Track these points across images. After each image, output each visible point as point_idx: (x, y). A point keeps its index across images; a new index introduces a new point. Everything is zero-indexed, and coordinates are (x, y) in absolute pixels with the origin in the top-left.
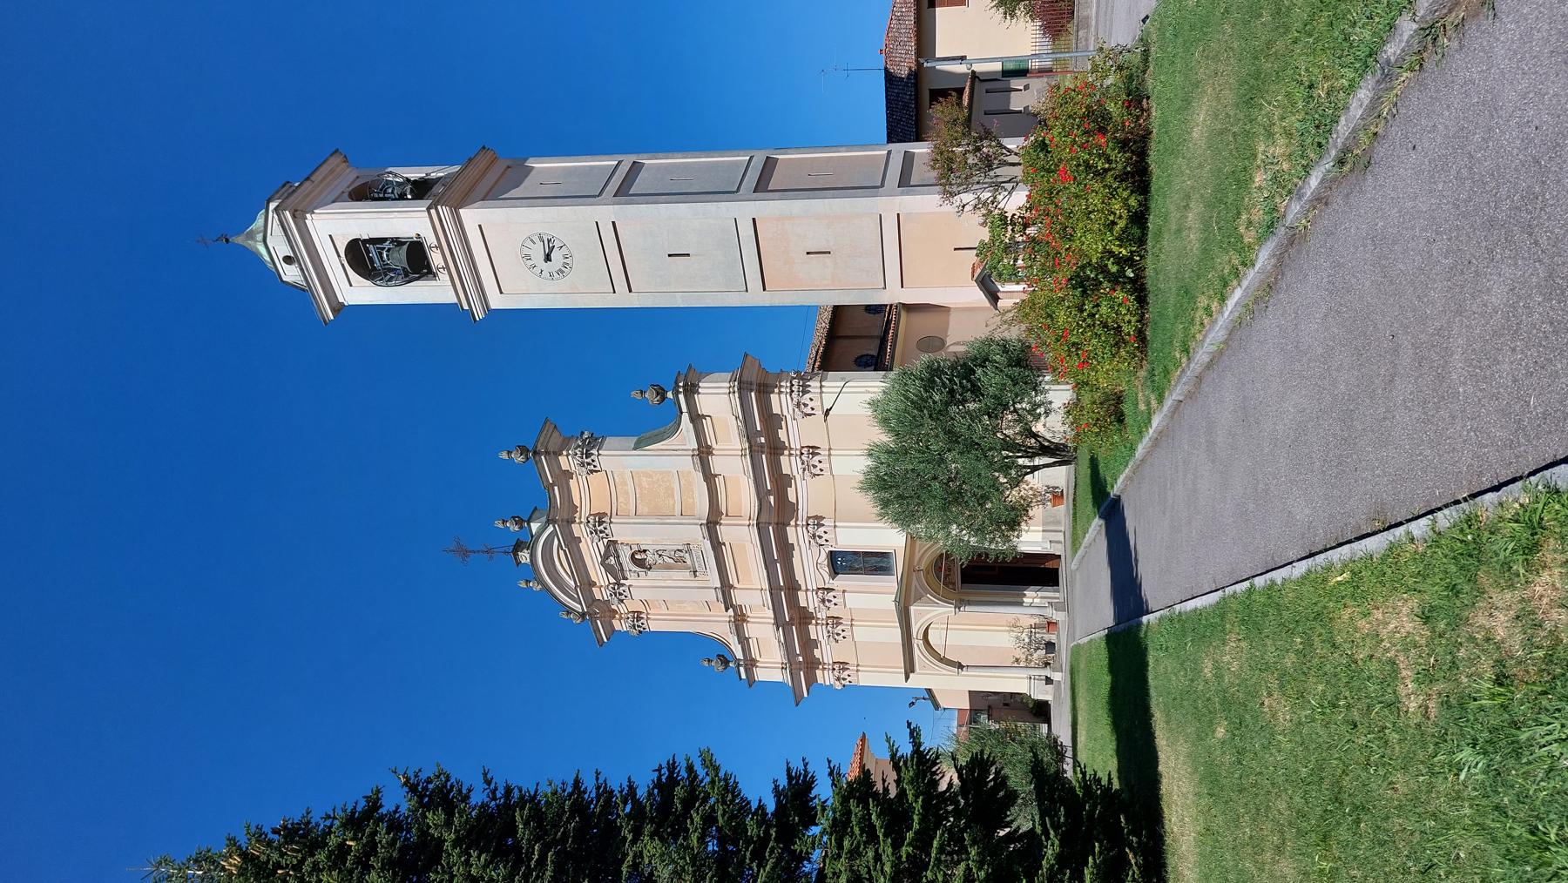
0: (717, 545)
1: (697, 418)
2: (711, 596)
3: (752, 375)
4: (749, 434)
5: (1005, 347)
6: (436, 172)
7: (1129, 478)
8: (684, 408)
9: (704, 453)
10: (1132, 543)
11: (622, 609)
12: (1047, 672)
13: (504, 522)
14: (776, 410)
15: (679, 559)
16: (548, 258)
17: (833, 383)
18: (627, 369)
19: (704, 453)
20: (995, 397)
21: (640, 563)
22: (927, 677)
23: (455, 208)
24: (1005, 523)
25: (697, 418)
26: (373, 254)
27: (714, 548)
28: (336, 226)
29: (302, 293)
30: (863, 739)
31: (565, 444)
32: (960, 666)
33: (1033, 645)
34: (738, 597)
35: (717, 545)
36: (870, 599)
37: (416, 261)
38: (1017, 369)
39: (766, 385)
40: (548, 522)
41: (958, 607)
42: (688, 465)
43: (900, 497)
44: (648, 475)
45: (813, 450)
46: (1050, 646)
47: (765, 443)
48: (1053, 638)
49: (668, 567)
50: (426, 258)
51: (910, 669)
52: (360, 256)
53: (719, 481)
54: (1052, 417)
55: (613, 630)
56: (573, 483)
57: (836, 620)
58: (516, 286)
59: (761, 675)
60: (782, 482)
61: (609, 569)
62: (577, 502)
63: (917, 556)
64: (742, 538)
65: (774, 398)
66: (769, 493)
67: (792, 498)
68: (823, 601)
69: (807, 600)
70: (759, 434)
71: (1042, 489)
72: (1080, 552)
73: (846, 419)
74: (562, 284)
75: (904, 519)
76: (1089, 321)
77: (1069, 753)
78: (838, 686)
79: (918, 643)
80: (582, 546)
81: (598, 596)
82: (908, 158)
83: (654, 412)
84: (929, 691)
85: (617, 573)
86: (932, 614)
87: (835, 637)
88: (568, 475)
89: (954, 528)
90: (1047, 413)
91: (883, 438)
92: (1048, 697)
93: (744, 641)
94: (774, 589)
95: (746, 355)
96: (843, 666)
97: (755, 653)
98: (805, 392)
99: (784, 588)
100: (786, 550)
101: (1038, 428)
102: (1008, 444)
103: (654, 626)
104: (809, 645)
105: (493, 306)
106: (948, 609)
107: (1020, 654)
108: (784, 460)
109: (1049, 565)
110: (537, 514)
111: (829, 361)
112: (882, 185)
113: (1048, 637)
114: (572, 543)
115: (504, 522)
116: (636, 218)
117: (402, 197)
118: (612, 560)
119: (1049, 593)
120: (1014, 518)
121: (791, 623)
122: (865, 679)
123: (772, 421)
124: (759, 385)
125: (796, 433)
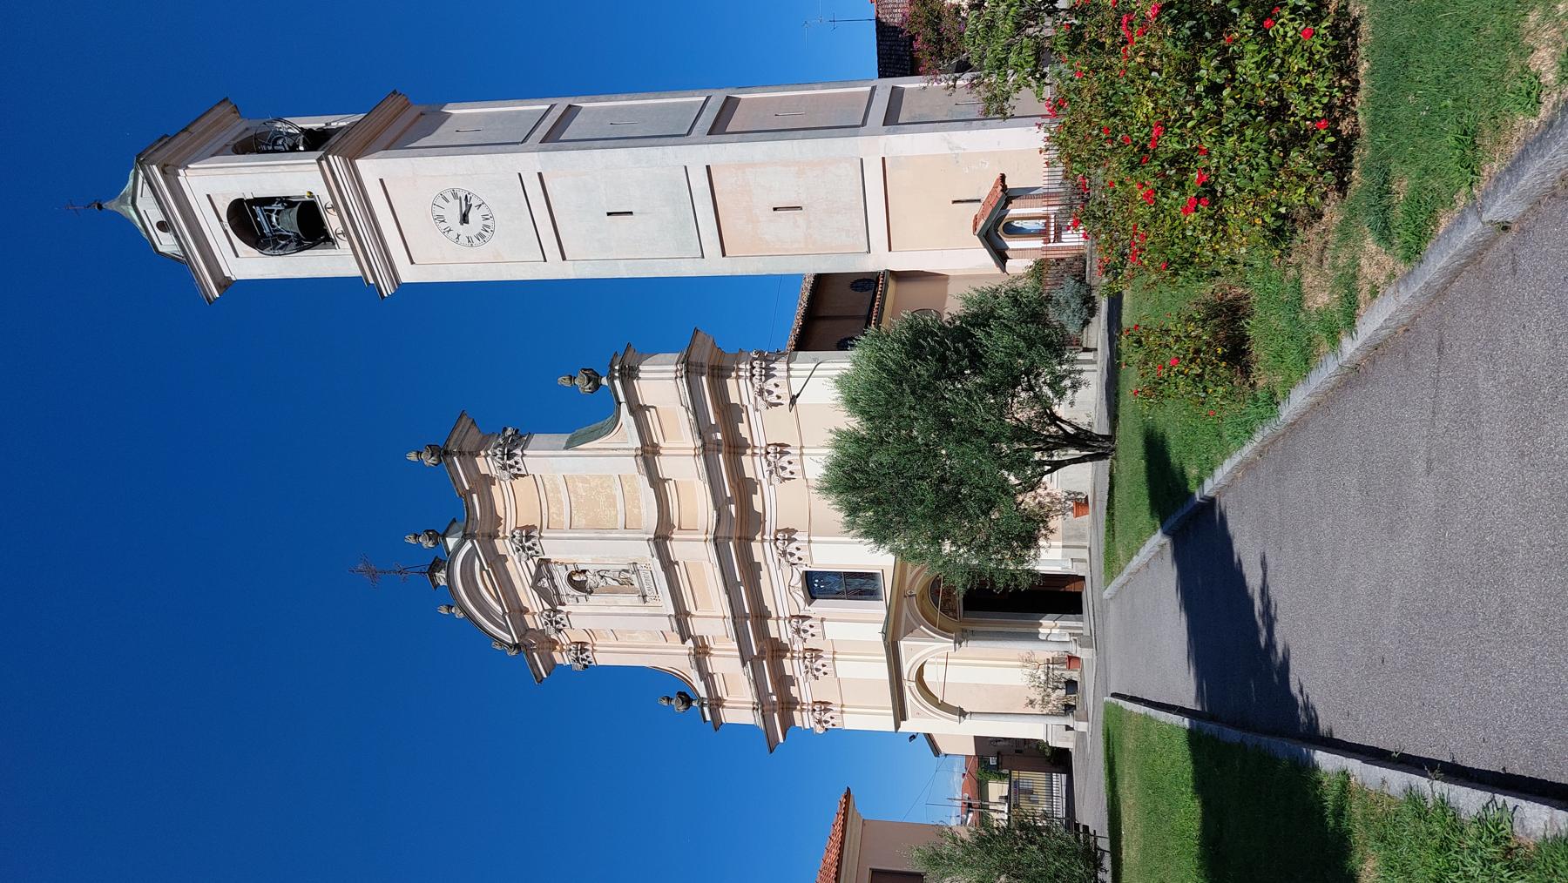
0: (668, 565)
1: (638, 410)
2: (666, 625)
3: (702, 355)
4: (702, 429)
5: (1015, 299)
6: (338, 121)
7: (1248, 466)
8: (622, 399)
9: (649, 453)
10: (1253, 581)
11: (563, 638)
12: (1070, 721)
13: (416, 536)
14: (734, 399)
15: (625, 581)
16: (464, 219)
17: (804, 363)
18: (555, 353)
19: (649, 453)
20: (1001, 366)
21: (580, 587)
22: (921, 720)
23: (351, 158)
24: (1018, 538)
25: (638, 410)
26: (261, 218)
27: (664, 568)
28: (214, 183)
29: (179, 266)
30: (848, 795)
31: (483, 444)
32: (962, 713)
33: (1050, 683)
34: (697, 627)
35: (668, 565)
36: (854, 629)
37: (309, 227)
38: (1033, 327)
39: (721, 368)
40: (465, 537)
41: (958, 641)
42: (631, 467)
43: (876, 502)
44: (584, 480)
45: (782, 449)
46: (1071, 685)
47: (723, 440)
48: (1075, 675)
49: (614, 591)
50: (323, 223)
51: (900, 714)
52: (246, 219)
53: (670, 487)
54: (1082, 391)
55: (554, 664)
56: (495, 489)
57: (816, 653)
58: (431, 256)
59: (729, 716)
60: (745, 488)
61: (543, 594)
62: (500, 513)
63: (909, 578)
64: (697, 556)
65: (731, 383)
66: (730, 501)
67: (758, 507)
68: (798, 631)
69: (779, 630)
70: (715, 428)
71: (1061, 495)
72: (1120, 580)
73: (810, 406)
74: (483, 251)
75: (879, 533)
76: (1208, 103)
77: (1107, 862)
78: (819, 730)
79: (910, 687)
80: (509, 565)
81: (531, 625)
82: (896, 96)
83: (584, 402)
84: (929, 737)
85: (551, 597)
86: (928, 651)
87: (813, 673)
88: (489, 480)
89: (947, 547)
90: (1075, 386)
91: (851, 422)
92: (1070, 745)
93: (706, 677)
94: (737, 617)
95: (696, 331)
96: (825, 706)
97: (721, 692)
98: (768, 376)
99: (750, 615)
100: (752, 571)
101: (1061, 410)
102: (1021, 433)
103: (602, 659)
104: (784, 682)
105: (404, 280)
106: (945, 645)
107: (1036, 695)
108: (746, 460)
109: (1071, 588)
110: (455, 526)
111: (805, 341)
112: (864, 123)
113: (1068, 674)
114: (497, 562)
115: (416, 536)
116: (569, 169)
117: (294, 149)
118: (545, 583)
119: (1070, 622)
120: (1028, 532)
121: (761, 656)
122: (851, 722)
123: (731, 414)
124: (712, 368)
125: (760, 427)
